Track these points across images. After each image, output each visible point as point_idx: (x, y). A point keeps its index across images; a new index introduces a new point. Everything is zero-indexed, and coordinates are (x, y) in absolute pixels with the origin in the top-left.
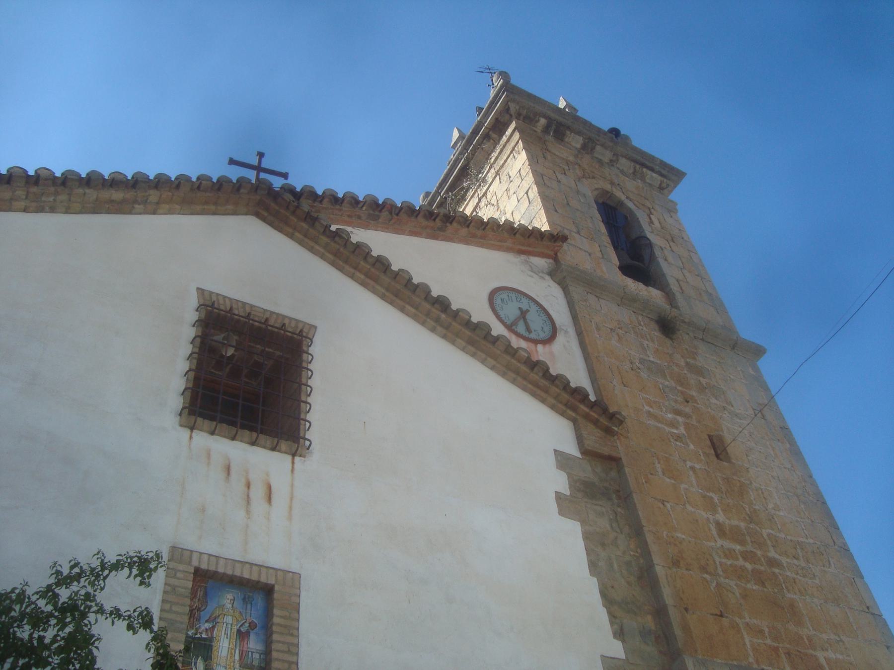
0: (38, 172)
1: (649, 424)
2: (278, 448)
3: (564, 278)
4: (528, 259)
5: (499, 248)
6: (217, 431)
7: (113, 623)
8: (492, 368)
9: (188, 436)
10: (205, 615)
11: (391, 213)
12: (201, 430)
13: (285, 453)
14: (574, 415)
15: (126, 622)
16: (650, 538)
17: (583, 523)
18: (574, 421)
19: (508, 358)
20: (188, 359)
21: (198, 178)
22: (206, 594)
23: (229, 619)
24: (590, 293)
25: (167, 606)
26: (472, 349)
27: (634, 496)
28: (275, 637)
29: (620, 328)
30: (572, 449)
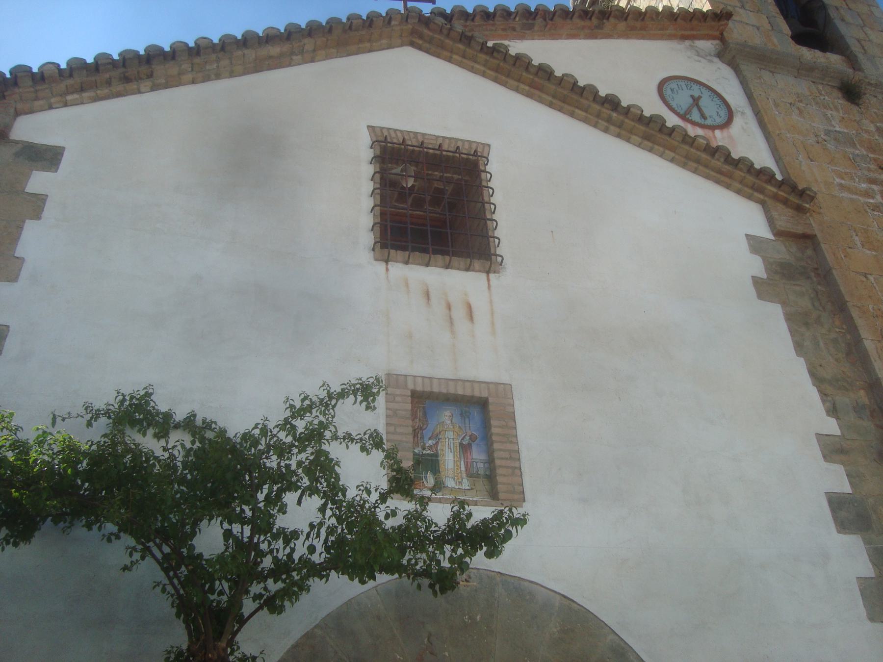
0: (198, 42)
1: (842, 197)
2: (472, 267)
3: (734, 57)
4: (692, 44)
5: (661, 37)
6: (411, 260)
7: (347, 447)
8: (672, 160)
9: (385, 268)
10: (427, 433)
11: (545, 20)
12: (396, 261)
13: (480, 271)
14: (761, 197)
15: (359, 445)
16: (855, 313)
17: (784, 304)
18: (763, 203)
19: (686, 147)
20: (371, 196)
21: (348, 19)
22: (425, 414)
23: (451, 435)
24: (764, 69)
25: (392, 429)
26: (650, 144)
27: (834, 272)
28: (496, 446)
29: (801, 101)
30: (763, 231)
